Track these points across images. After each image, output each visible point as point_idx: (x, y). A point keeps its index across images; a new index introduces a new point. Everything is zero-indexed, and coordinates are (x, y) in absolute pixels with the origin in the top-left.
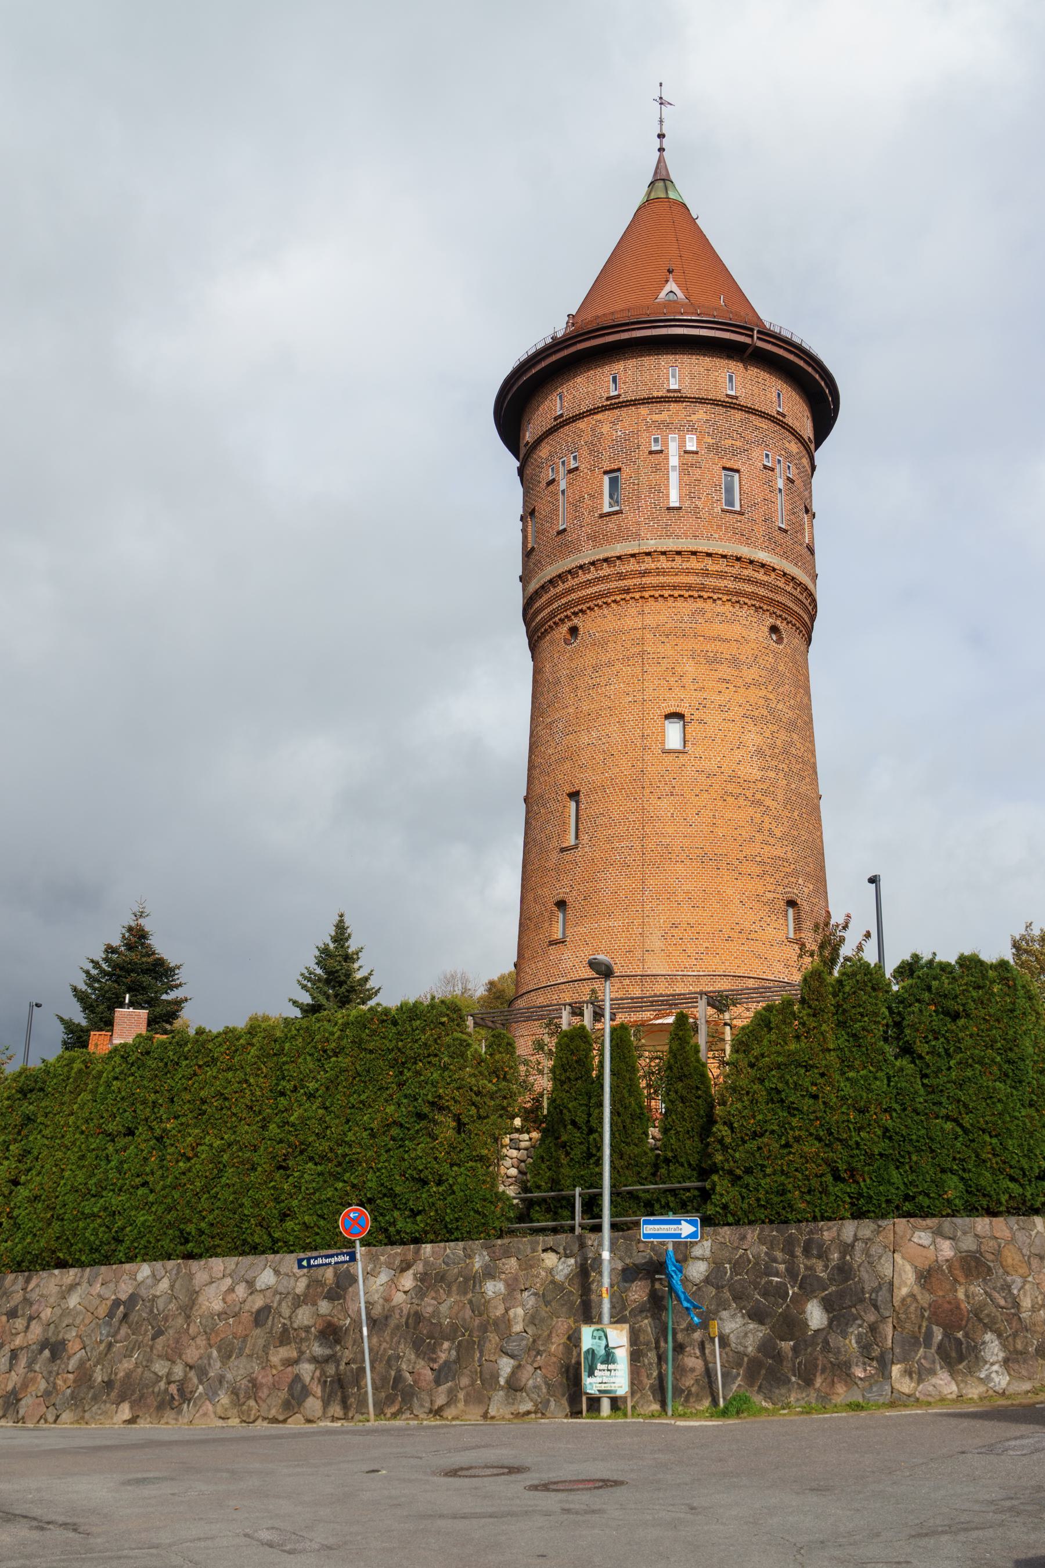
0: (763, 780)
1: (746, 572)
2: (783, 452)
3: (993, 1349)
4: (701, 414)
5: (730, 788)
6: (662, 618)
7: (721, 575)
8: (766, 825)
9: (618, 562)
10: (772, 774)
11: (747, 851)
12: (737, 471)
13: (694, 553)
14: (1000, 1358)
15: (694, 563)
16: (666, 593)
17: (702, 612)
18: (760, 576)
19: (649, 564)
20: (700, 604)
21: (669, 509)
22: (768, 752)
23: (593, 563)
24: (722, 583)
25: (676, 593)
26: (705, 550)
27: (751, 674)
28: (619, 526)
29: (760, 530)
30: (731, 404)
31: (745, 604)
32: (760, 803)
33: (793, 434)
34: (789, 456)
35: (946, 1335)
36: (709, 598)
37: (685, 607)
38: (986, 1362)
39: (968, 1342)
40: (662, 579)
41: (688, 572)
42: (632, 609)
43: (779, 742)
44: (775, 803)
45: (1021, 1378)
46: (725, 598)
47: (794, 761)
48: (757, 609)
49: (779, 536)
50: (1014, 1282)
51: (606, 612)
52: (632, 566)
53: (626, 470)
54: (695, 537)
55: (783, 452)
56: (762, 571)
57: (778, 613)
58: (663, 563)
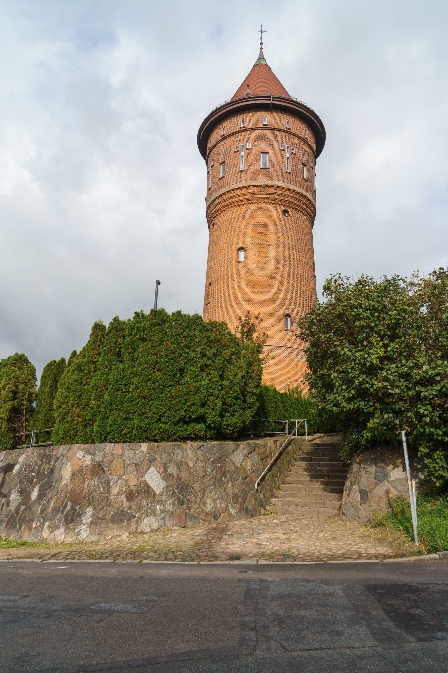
0: (276, 269)
1: (270, 191)
2: (290, 143)
3: (88, 516)
4: (253, 134)
5: (261, 273)
6: (238, 213)
7: (260, 193)
8: (276, 286)
9: (224, 196)
10: (281, 267)
11: (267, 297)
12: (268, 153)
13: (249, 186)
14: (89, 522)
15: (249, 190)
16: (240, 204)
17: (253, 208)
18: (278, 191)
19: (234, 194)
20: (252, 205)
21: (240, 171)
22: (279, 258)
23: (216, 198)
24: (260, 196)
25: (243, 203)
26: (253, 184)
27: (272, 229)
28: (224, 182)
29: (277, 174)
30: (265, 128)
31: (271, 203)
32: (274, 278)
33: (296, 136)
34: (293, 144)
35: (72, 507)
36: (256, 202)
37: (246, 208)
38: (82, 523)
39: (79, 512)
40: (238, 198)
41: (247, 194)
42: (229, 212)
43: (285, 254)
44: (281, 278)
45: (95, 534)
46: (262, 202)
47: (292, 261)
48: (277, 204)
49: (287, 175)
50: (112, 478)
51: (221, 215)
52: (228, 195)
53: (227, 161)
54: (249, 180)
55: (290, 143)
56: (278, 189)
57: (287, 205)
58: (238, 192)
